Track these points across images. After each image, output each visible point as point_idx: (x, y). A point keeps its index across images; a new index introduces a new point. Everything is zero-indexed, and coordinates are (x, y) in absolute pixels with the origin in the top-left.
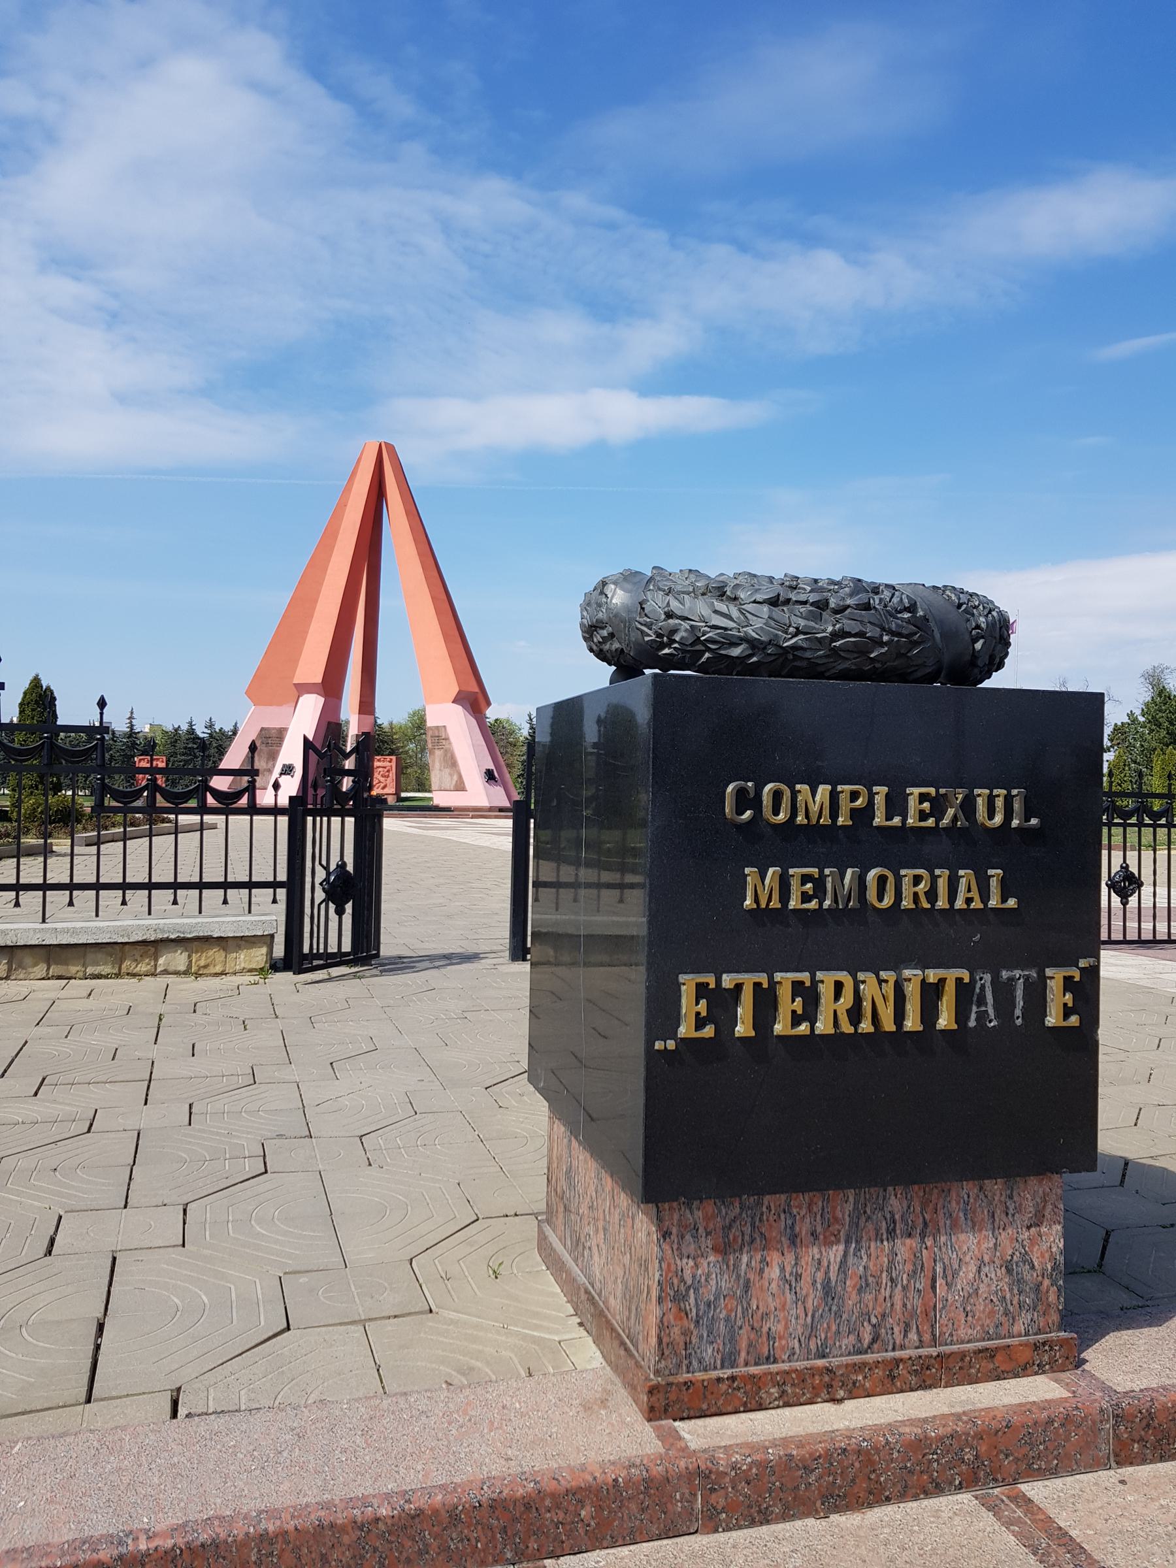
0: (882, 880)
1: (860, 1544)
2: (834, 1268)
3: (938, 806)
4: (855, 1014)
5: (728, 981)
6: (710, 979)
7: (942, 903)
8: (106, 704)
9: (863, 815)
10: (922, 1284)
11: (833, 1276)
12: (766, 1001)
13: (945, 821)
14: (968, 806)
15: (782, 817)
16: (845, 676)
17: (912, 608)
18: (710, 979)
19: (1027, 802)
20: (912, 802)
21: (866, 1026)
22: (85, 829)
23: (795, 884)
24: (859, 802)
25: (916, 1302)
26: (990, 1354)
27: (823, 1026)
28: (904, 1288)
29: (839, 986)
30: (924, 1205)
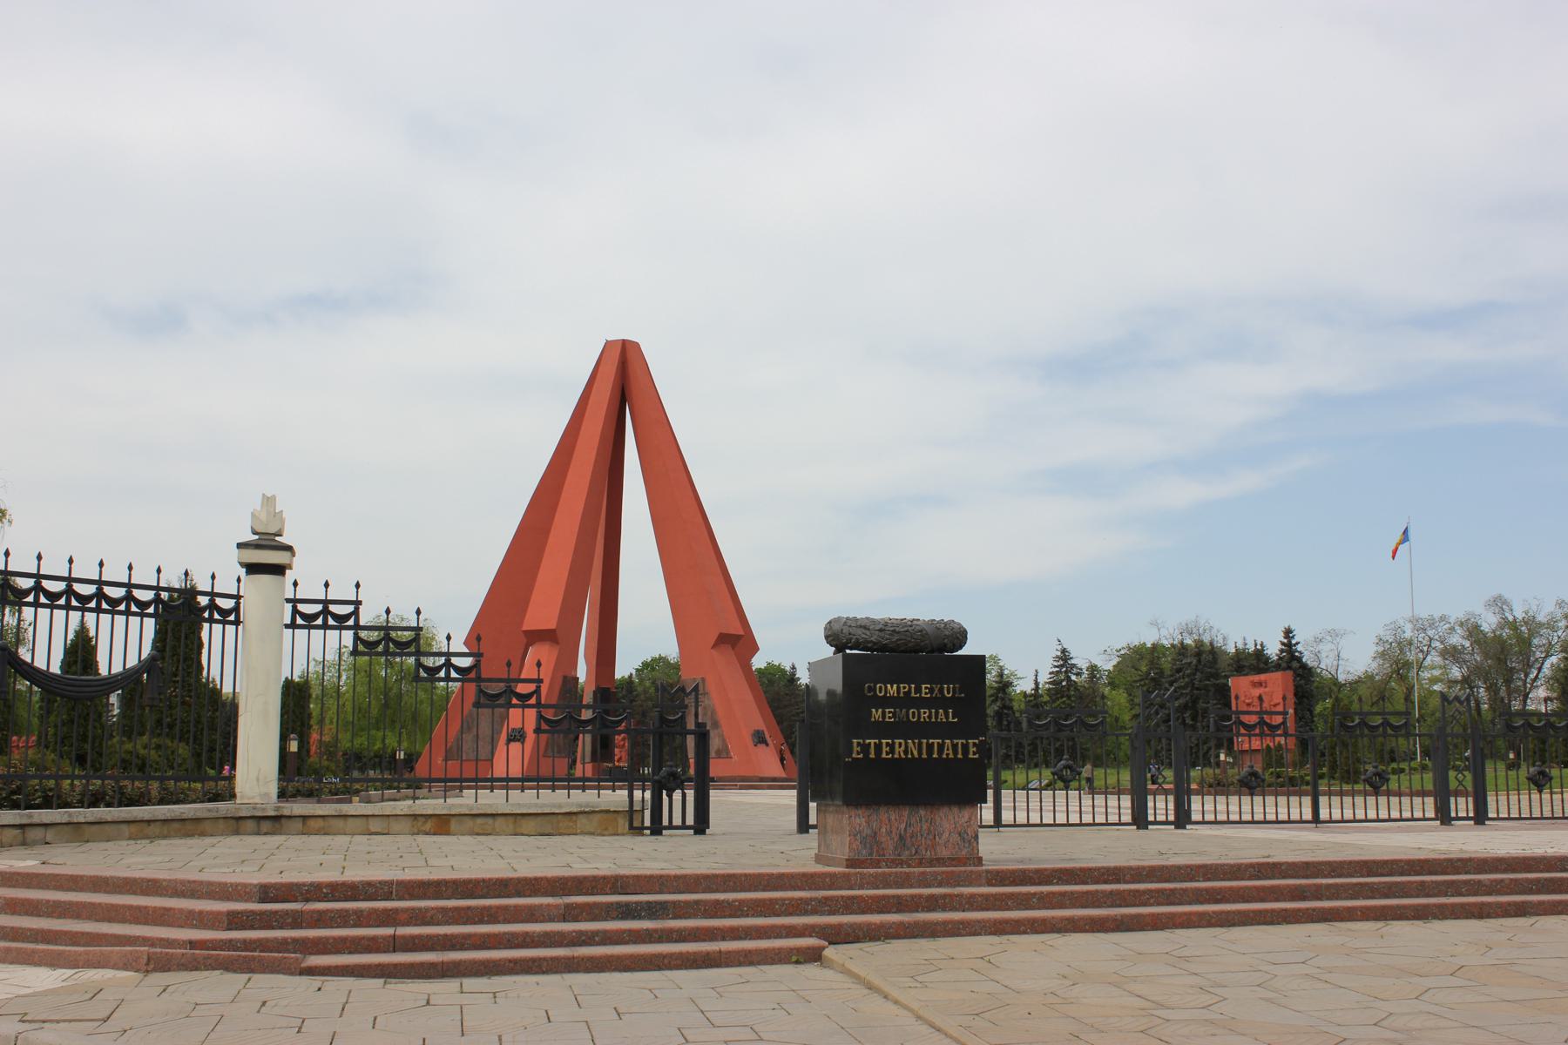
0: (914, 713)
1: (1273, 780)
2: (902, 830)
3: (931, 690)
4: (906, 752)
5: (868, 741)
6: (861, 741)
7: (933, 720)
8: (477, 638)
9: (908, 694)
10: (931, 837)
11: (902, 832)
12: (941, 747)
13: (934, 695)
14: (941, 690)
15: (882, 694)
16: (902, 652)
17: (921, 631)
18: (861, 741)
19: (960, 689)
20: (924, 690)
21: (910, 756)
22: (348, 678)
23: (887, 715)
24: (906, 690)
25: (929, 842)
26: (953, 859)
27: (896, 756)
28: (925, 838)
29: (900, 744)
30: (931, 812)
